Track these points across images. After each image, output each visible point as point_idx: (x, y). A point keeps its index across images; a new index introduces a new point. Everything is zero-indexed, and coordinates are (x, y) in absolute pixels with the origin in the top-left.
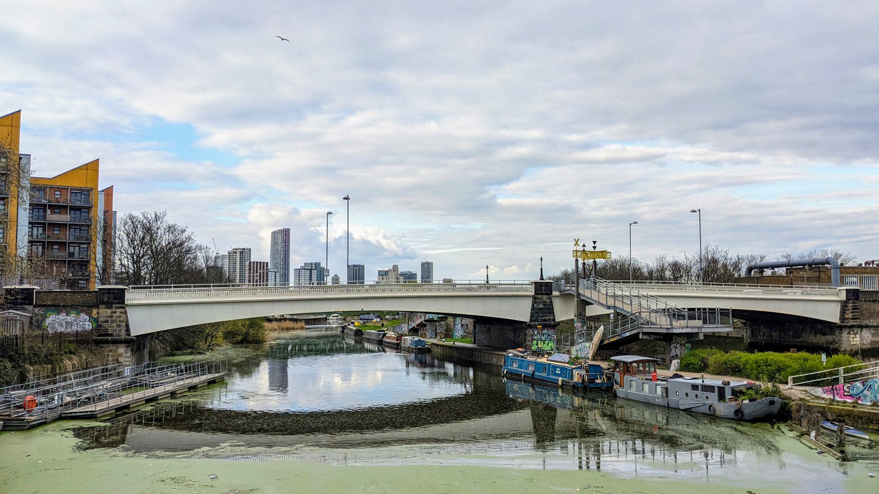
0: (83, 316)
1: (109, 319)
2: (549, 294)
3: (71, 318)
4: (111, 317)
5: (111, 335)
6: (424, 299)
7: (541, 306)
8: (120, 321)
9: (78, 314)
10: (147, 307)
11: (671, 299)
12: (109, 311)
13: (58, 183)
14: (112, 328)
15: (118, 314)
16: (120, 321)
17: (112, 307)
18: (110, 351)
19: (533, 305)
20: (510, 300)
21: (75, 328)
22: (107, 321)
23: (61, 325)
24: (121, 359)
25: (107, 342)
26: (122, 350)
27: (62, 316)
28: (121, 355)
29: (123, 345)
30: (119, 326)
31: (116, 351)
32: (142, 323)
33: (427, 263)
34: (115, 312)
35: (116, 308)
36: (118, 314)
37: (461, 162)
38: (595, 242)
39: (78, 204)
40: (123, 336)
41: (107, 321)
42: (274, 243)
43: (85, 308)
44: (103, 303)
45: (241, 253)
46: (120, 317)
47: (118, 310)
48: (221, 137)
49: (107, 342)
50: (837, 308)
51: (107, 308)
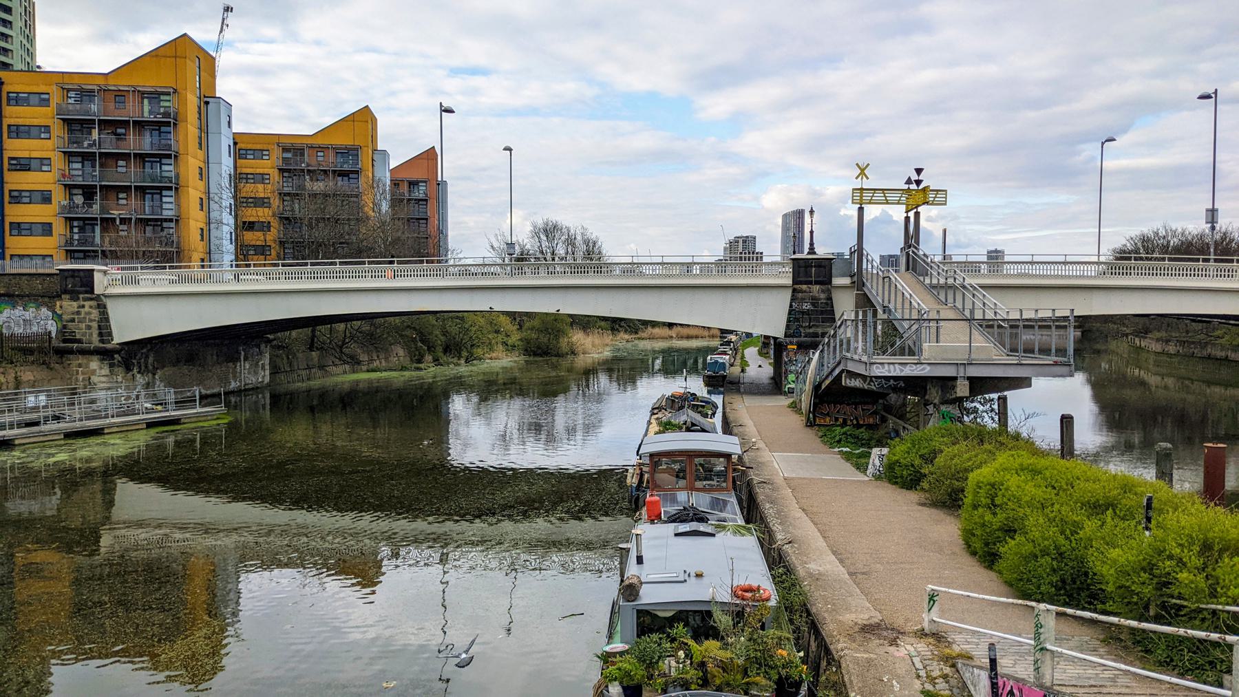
0: (44, 311)
1: (76, 317)
2: (826, 281)
3: (30, 313)
4: (78, 313)
5: (79, 341)
6: (708, 292)
7: (807, 306)
8: (91, 321)
9: (37, 308)
10: (163, 299)
11: (998, 293)
12: (75, 304)
13: (319, 141)
14: (80, 330)
15: (87, 309)
16: (91, 321)
17: (78, 299)
18: (80, 366)
19: (791, 306)
20: (745, 293)
21: (35, 329)
22: (73, 320)
23: (19, 325)
24: (95, 379)
25: (71, 352)
26: (94, 364)
27: (19, 311)
28: (93, 372)
29: (96, 358)
30: (89, 327)
31: (87, 366)
32: (130, 324)
33: (996, 251)
34: (83, 306)
35: (85, 300)
36: (87, 309)
37: (1032, 114)
38: (919, 171)
39: (346, 167)
40: (95, 342)
41: (73, 320)
42: (785, 228)
43: (46, 300)
44: (66, 292)
45: (744, 242)
46: (89, 313)
47: (87, 304)
48: (718, 105)
49: (71, 352)
50: (118, 513)
51: (72, 299)
